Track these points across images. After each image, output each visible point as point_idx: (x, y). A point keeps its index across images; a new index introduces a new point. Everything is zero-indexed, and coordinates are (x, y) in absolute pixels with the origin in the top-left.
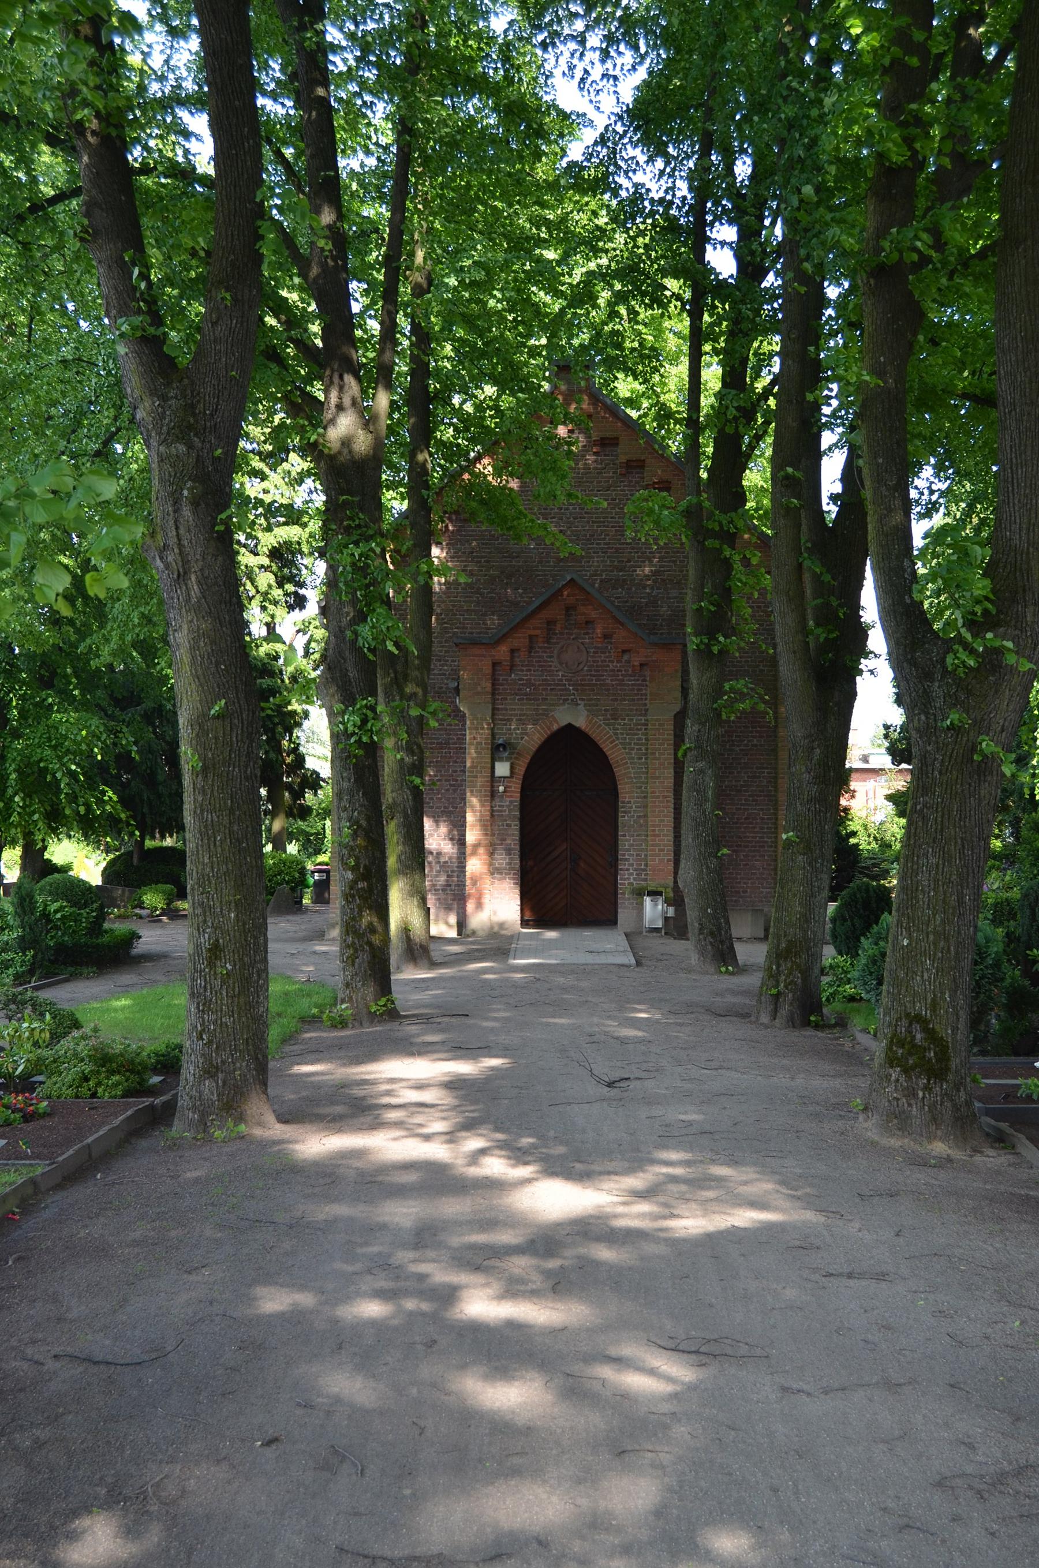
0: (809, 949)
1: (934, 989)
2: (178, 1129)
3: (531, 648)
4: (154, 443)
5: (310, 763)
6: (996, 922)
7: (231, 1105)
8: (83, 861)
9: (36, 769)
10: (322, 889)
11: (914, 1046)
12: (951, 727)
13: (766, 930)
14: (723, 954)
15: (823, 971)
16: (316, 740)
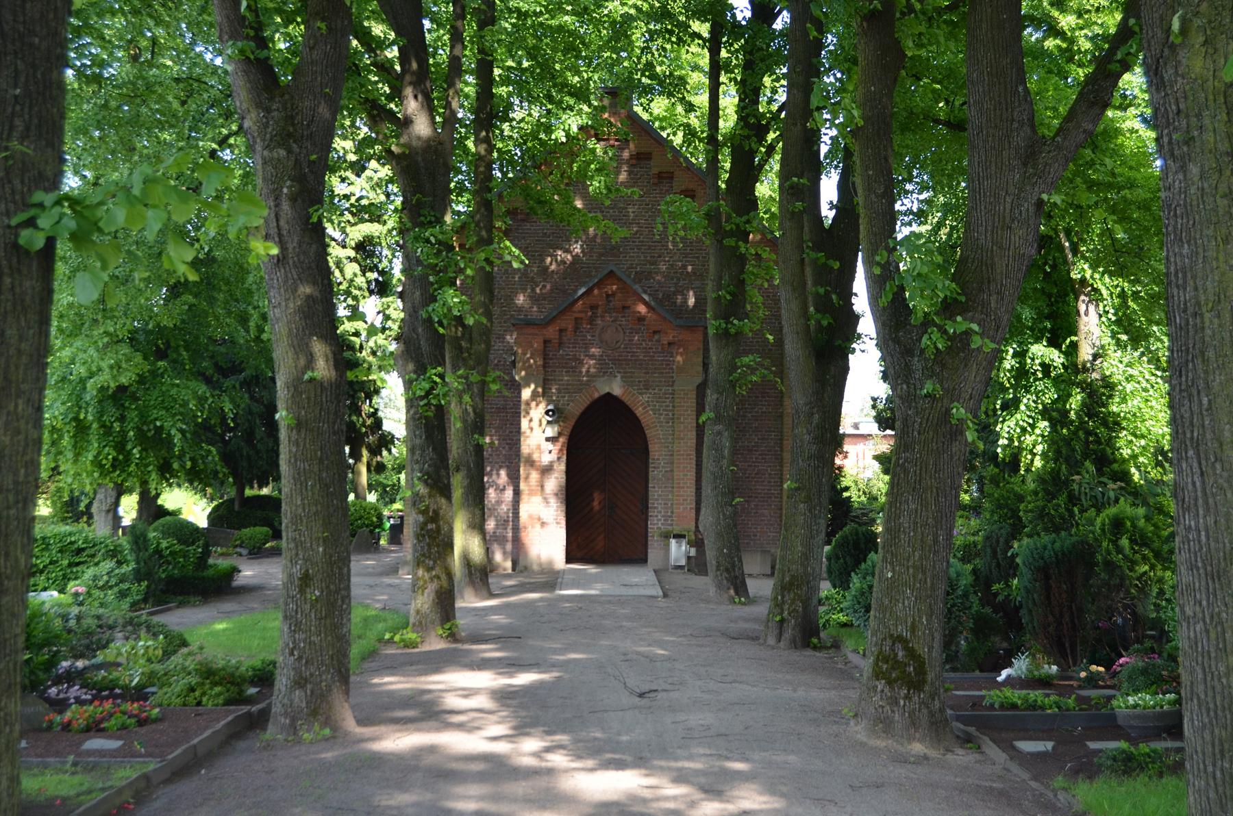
0: (808, 582)
1: (914, 615)
2: (272, 732)
3: (576, 329)
4: (258, 148)
5: (387, 426)
6: (964, 560)
7: (318, 709)
8: (191, 506)
9: (152, 427)
10: (397, 531)
11: (897, 662)
12: (928, 395)
13: (773, 568)
14: (739, 586)
15: (820, 602)
16: (392, 406)
